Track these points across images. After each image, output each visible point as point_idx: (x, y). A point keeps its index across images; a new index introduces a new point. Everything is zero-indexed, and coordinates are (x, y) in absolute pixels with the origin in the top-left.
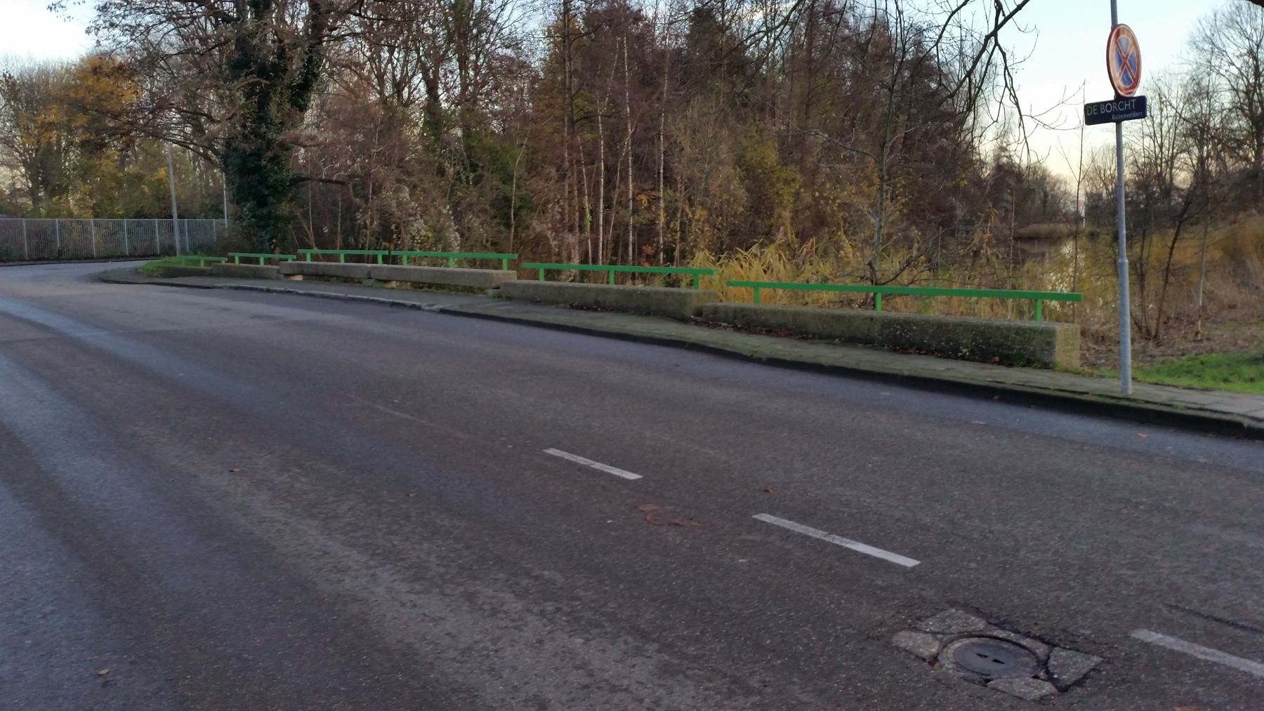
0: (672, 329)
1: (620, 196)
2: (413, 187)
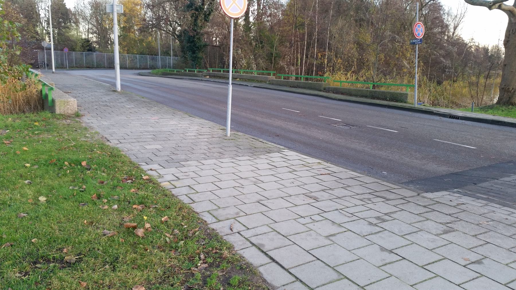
0: (316, 92)
1: (312, 53)
2: (242, 49)
